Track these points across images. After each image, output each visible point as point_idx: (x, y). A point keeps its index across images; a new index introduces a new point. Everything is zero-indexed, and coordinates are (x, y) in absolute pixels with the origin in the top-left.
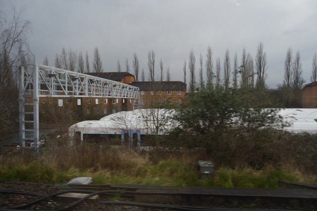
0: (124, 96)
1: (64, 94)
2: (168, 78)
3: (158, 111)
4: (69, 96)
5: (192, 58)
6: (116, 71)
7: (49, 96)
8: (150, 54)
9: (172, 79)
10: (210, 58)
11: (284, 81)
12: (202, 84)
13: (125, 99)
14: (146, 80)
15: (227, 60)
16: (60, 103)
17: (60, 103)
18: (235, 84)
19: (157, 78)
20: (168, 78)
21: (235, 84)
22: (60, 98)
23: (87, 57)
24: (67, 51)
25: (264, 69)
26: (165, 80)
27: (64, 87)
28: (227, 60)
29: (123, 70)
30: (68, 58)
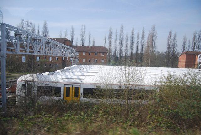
0: (63, 55)
1: (26, 51)
2: (94, 44)
3: (189, 50)
4: (30, 54)
5: (111, 32)
6: (59, 37)
7: (33, 54)
8: (82, 27)
9: (96, 45)
10: (122, 32)
11: (44, 82)
12: (126, 52)
13: (65, 57)
14: (79, 45)
15: (133, 34)
16: (24, 60)
17: (24, 60)
18: (137, 51)
19: (86, 44)
20: (94, 44)
21: (137, 51)
22: (24, 55)
23: (39, 27)
24: (25, 21)
25: (155, 42)
26: (91, 45)
27: (27, 46)
28: (133, 34)
29: (63, 37)
30: (25, 26)
